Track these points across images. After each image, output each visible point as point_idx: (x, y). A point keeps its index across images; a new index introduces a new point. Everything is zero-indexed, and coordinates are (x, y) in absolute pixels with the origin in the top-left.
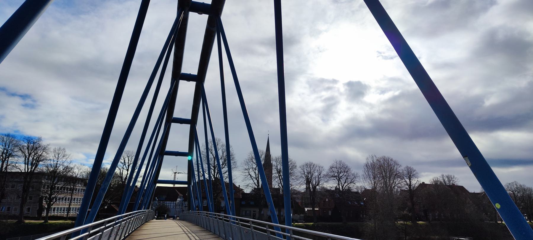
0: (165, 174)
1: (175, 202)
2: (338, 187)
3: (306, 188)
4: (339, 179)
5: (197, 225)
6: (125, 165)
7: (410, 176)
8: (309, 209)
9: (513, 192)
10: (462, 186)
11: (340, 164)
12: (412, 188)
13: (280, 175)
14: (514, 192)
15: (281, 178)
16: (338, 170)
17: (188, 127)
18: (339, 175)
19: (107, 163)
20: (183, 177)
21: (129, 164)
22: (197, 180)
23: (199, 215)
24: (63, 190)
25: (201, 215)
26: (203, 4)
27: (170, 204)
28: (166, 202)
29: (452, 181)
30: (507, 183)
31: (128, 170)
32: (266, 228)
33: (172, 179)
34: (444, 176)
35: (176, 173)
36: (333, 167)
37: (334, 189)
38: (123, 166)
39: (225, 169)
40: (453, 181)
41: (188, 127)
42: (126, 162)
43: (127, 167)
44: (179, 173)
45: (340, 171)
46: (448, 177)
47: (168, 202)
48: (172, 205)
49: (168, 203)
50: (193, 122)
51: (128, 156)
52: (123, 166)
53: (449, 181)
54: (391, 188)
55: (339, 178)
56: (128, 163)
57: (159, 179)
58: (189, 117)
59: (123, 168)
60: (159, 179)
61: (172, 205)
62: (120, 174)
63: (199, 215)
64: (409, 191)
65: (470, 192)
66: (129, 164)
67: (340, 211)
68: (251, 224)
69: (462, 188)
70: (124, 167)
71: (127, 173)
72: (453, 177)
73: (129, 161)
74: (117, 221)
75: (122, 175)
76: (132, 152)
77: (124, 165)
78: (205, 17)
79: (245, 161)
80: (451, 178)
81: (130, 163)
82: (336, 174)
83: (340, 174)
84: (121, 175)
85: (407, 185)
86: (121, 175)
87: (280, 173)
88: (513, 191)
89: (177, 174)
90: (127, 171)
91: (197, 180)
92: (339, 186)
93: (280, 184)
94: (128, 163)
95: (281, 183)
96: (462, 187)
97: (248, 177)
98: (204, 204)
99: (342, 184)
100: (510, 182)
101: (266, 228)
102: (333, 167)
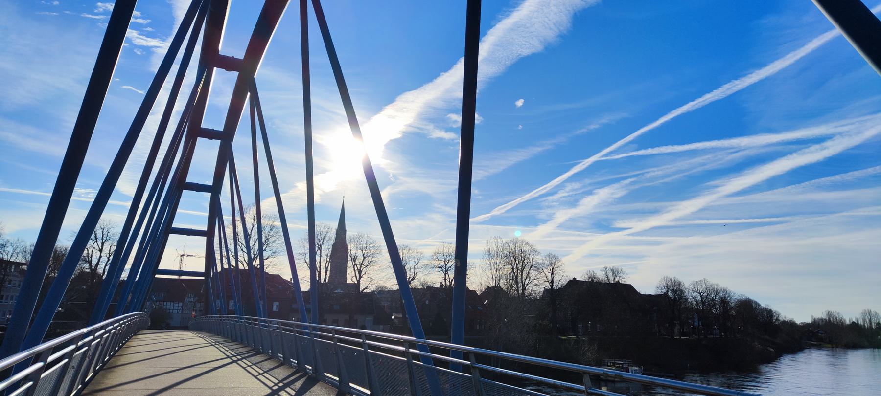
0: (169, 261)
1: (181, 304)
2: (444, 283)
3: (610, 283)
4: (446, 271)
5: (218, 335)
6: (96, 242)
7: (553, 269)
8: (398, 316)
9: (700, 294)
10: (630, 285)
11: (449, 249)
12: (554, 287)
13: (355, 264)
14: (702, 294)
15: (356, 269)
16: (445, 257)
17: (204, 239)
18: (446, 265)
19: (65, 240)
20: (199, 265)
21: (104, 241)
22: (219, 269)
23: (221, 320)
24: (9, 284)
25: (224, 320)
26: (232, 59)
27: (174, 307)
28: (165, 303)
29: (618, 277)
30: (694, 281)
31: (101, 251)
32: (292, 328)
33: (177, 268)
34: (607, 269)
35: (183, 255)
36: (438, 253)
37: (438, 286)
38: (93, 244)
39: (257, 263)
40: (620, 277)
41: (204, 239)
42: (98, 237)
43: (100, 245)
44: (188, 256)
45: (448, 259)
46: (613, 271)
47: (169, 304)
48: (176, 308)
49: (168, 305)
50: (215, 189)
51: (103, 227)
52: (93, 244)
53: (615, 276)
54: (523, 285)
55: (446, 269)
56: (102, 239)
57: (160, 267)
58: (210, 182)
59: (93, 248)
60: (160, 267)
61: (176, 308)
62: (88, 256)
63: (221, 320)
64: (550, 291)
65: (642, 293)
66: (104, 241)
67: (445, 320)
68: (474, 361)
69: (629, 287)
70: (95, 245)
71: (99, 255)
72: (620, 270)
73: (103, 235)
74: (125, 320)
75: (91, 259)
76: (110, 221)
77: (94, 242)
78: (217, 143)
79: (299, 241)
80: (618, 272)
81: (105, 239)
82: (442, 264)
83: (448, 263)
84: (89, 259)
85: (548, 281)
86: (90, 259)
87: (355, 261)
88: (700, 293)
89: (184, 257)
90: (99, 253)
91: (219, 269)
92: (445, 281)
93: (355, 277)
94: (102, 239)
95: (356, 276)
96: (630, 286)
97: (304, 266)
98: (230, 306)
99: (449, 278)
100: (698, 280)
101: (292, 328)
102: (438, 253)
